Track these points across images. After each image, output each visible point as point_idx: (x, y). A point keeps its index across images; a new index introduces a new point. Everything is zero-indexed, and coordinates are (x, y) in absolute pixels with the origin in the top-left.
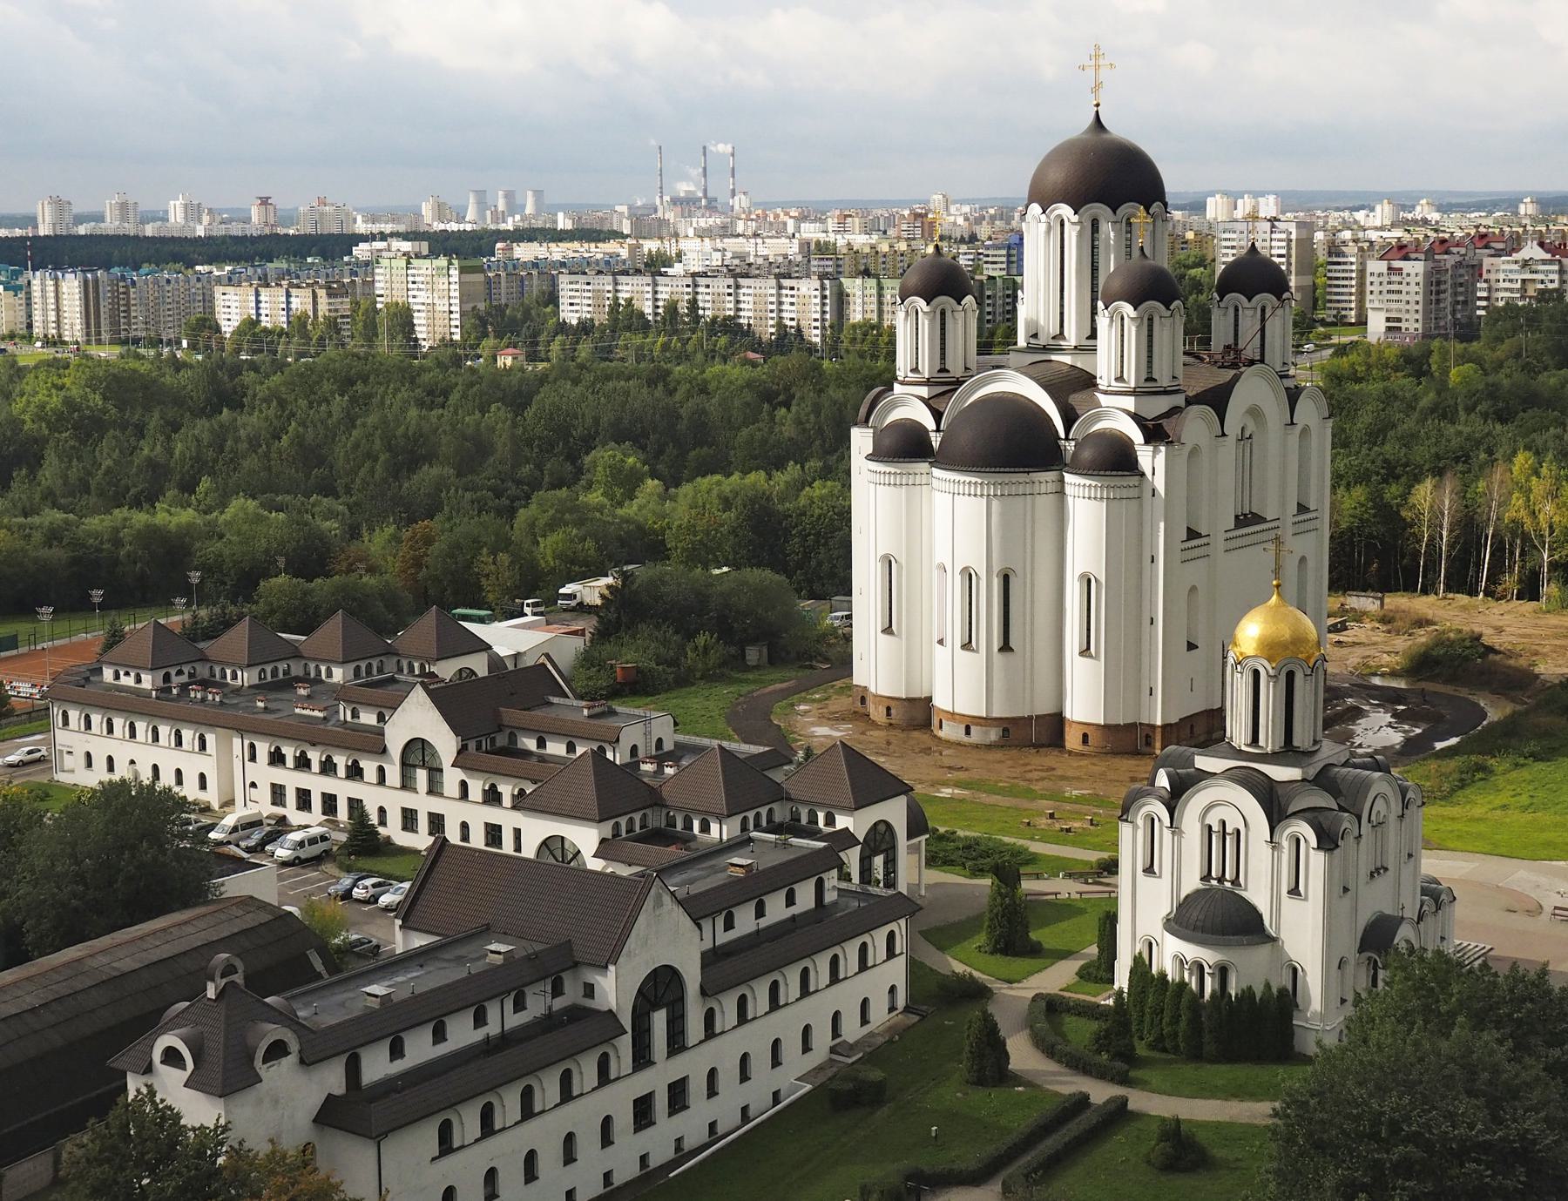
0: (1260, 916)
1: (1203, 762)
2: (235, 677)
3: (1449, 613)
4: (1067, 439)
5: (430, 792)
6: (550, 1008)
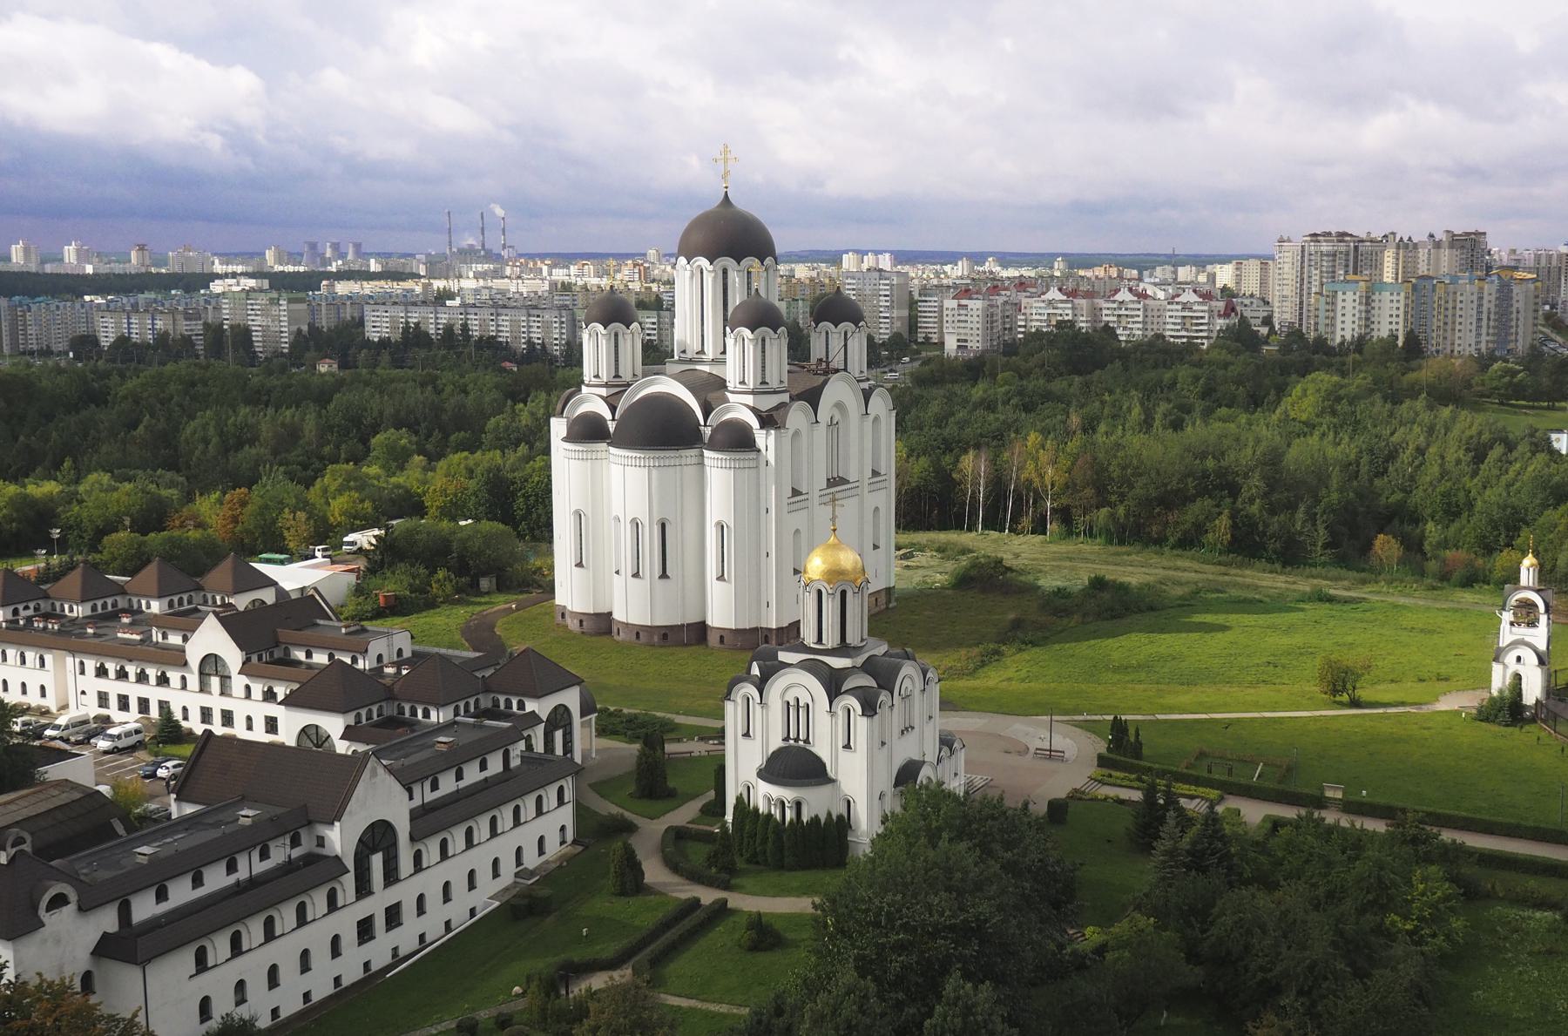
1: (783, 656)
2: (71, 610)
3: (982, 543)
5: (222, 694)
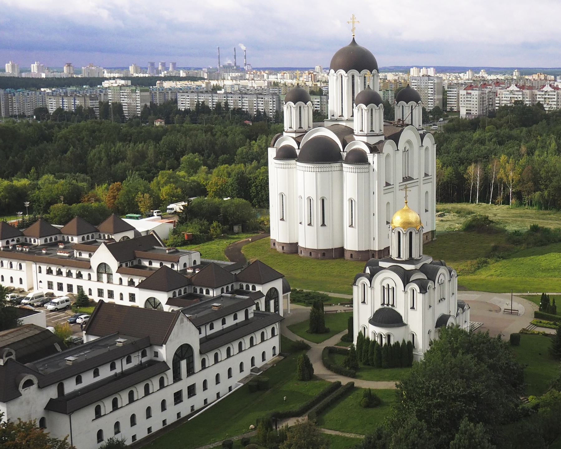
0: (401, 317)
1: (381, 264)
2: (35, 242)
3: (478, 208)
4: (343, 152)
5: (108, 282)
6: (141, 361)
